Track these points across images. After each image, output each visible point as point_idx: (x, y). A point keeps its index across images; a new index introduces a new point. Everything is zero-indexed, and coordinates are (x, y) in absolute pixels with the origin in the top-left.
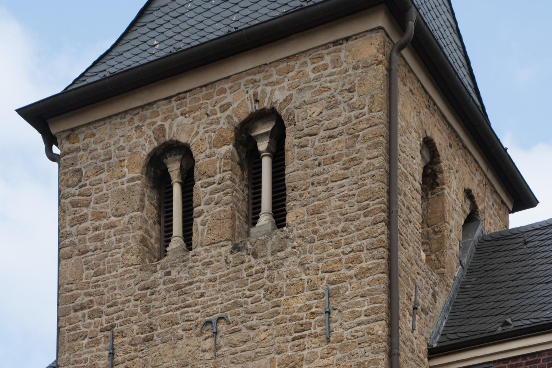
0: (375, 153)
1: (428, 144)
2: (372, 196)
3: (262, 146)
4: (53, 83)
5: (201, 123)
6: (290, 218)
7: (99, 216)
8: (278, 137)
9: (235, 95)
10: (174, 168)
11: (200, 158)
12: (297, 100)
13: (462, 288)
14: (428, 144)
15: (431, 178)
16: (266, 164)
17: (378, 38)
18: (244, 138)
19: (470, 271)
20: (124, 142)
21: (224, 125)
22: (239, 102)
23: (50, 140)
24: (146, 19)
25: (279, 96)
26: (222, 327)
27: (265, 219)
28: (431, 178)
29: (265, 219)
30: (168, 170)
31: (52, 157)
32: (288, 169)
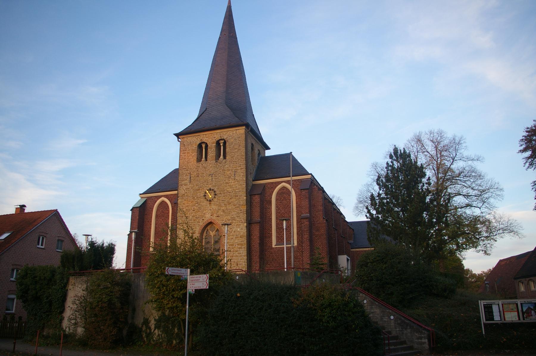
0: (246, 282)
1: (252, 144)
2: (242, 155)
3: (222, 144)
4: (178, 132)
5: (210, 138)
6: (227, 158)
7: (188, 153)
8: (225, 143)
9: (217, 135)
10: (204, 146)
11: (209, 146)
12: (229, 138)
13: (258, 167)
14: (252, 144)
15: (252, 149)
16: (222, 147)
17: (244, 130)
18: (218, 143)
19: (259, 164)
20: (195, 139)
21: (215, 141)
22: (218, 137)
23: (178, 138)
24: (201, 117)
25: (225, 137)
26: (213, 175)
27: (222, 157)
28: (252, 149)
29: (222, 157)
30: (202, 147)
31: (179, 141)
32: (227, 150)
